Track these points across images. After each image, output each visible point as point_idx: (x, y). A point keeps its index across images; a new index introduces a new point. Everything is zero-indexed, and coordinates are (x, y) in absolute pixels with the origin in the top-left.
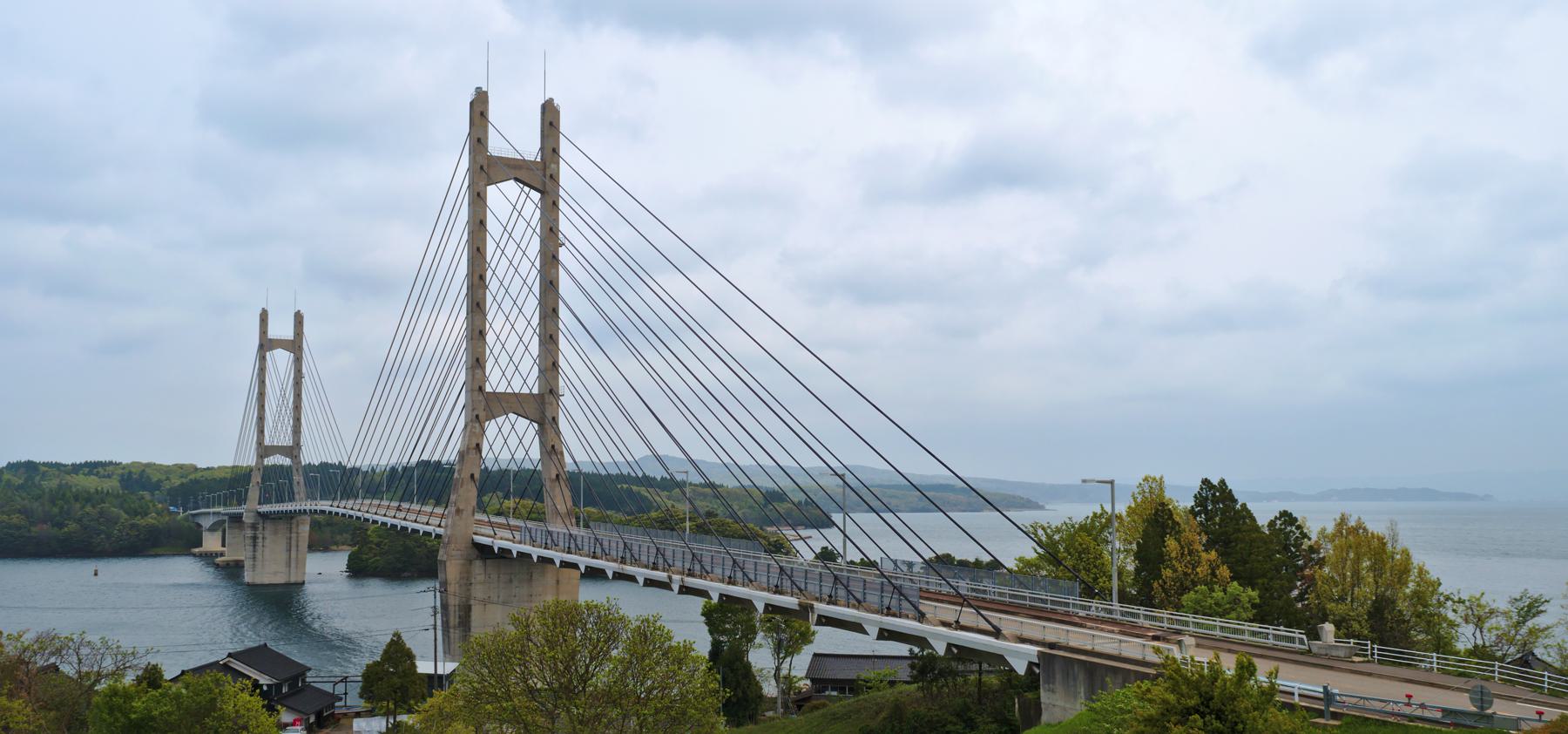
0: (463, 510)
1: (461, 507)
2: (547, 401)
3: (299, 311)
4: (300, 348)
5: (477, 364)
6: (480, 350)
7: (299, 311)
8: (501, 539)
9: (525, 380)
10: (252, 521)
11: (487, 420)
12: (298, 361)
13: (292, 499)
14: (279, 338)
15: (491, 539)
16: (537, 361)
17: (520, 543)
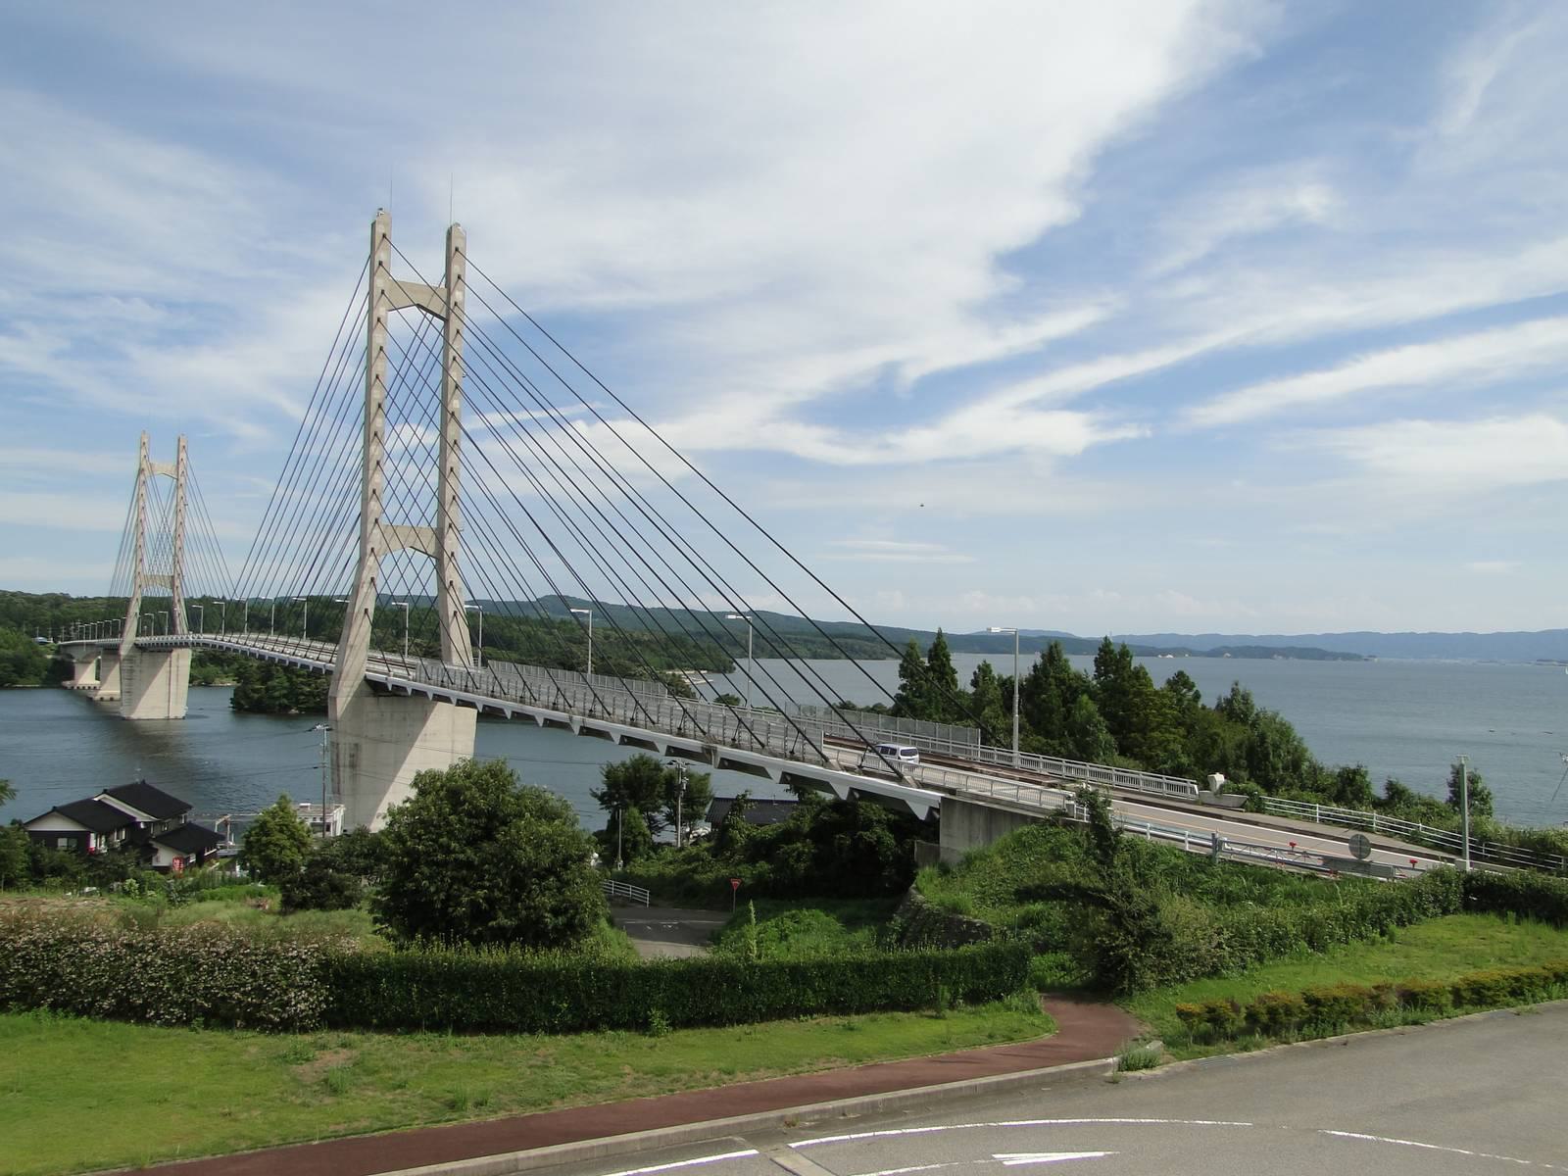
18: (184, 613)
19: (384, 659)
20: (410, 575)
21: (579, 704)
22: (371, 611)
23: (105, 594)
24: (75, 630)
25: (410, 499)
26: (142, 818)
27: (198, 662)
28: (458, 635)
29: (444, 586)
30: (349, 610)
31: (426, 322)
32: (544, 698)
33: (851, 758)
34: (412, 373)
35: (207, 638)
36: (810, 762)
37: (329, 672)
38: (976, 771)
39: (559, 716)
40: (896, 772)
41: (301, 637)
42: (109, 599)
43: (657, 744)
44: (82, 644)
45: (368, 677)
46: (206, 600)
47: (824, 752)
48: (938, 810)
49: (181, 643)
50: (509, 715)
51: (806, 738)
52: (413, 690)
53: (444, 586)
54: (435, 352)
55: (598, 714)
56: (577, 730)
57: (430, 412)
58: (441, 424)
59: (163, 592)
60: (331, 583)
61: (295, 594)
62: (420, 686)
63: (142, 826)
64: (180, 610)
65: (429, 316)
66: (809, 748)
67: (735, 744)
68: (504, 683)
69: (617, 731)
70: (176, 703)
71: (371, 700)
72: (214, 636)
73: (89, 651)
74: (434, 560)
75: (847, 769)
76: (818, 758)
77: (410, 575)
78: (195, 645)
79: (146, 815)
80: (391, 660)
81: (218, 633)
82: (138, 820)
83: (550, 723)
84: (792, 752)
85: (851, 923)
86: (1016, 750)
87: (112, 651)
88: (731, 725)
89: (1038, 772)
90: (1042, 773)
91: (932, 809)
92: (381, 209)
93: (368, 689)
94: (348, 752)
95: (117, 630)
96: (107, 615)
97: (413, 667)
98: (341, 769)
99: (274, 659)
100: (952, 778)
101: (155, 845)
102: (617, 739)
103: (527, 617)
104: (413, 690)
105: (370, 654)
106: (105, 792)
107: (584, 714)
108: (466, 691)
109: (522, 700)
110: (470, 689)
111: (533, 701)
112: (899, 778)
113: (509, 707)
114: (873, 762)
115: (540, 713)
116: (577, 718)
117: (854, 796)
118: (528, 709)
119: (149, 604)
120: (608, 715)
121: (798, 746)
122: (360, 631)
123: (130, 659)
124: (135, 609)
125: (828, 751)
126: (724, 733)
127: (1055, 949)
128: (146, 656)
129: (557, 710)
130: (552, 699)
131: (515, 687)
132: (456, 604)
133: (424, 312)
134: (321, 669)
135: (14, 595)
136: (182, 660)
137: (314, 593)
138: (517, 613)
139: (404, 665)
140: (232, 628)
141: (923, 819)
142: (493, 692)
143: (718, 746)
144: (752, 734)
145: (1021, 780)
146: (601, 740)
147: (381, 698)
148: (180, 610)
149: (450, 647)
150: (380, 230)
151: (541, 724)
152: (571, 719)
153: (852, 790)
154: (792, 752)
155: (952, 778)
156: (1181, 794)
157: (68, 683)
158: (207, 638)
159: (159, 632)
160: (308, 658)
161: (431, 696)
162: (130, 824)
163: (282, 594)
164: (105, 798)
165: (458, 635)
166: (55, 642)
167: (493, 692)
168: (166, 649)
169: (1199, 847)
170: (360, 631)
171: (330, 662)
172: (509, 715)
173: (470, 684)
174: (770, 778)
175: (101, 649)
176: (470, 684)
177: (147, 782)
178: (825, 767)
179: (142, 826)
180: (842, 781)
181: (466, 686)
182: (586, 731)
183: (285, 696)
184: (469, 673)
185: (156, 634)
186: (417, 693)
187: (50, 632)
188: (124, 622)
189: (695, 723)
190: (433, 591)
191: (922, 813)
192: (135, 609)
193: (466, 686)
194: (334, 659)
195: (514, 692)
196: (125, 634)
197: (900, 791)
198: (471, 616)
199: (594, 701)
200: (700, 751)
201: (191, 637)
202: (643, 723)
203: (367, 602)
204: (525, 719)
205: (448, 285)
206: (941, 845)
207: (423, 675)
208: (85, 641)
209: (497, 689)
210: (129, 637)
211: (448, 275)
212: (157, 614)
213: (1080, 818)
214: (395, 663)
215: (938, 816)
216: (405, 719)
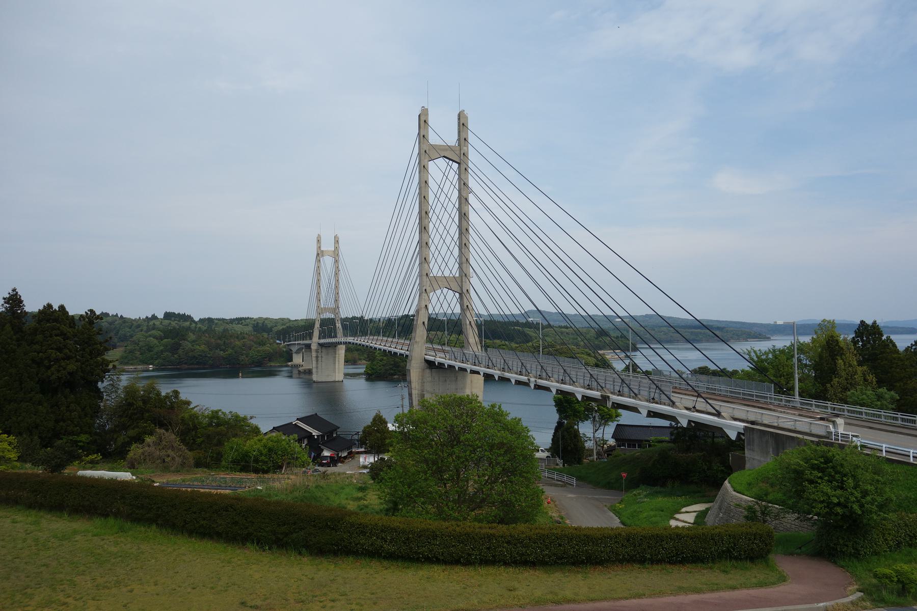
18: (340, 327)
20: (445, 306)
21: (534, 372)
22: (426, 323)
24: (293, 336)
25: (444, 264)
26: (315, 433)
28: (472, 337)
29: (465, 308)
30: (415, 323)
32: (515, 369)
33: (689, 401)
34: (443, 196)
36: (665, 404)
37: (407, 356)
38: (770, 410)
39: (523, 378)
40: (716, 411)
43: (576, 394)
44: (295, 344)
47: (672, 398)
48: (743, 434)
50: (497, 378)
51: (661, 391)
52: (459, 368)
53: (465, 308)
55: (545, 377)
56: (532, 386)
57: (452, 216)
59: (328, 315)
60: (407, 308)
62: (452, 363)
63: (316, 437)
64: (339, 325)
66: (663, 396)
67: (620, 394)
69: (554, 387)
70: (339, 373)
71: (428, 371)
73: (299, 347)
75: (687, 409)
76: (667, 401)
77: (445, 306)
78: (345, 343)
79: (316, 431)
82: (313, 434)
83: (518, 383)
84: (653, 399)
86: (797, 396)
87: (308, 347)
88: (645, 387)
89: (813, 410)
90: (815, 411)
91: (739, 434)
92: (423, 107)
96: (304, 329)
99: (397, 353)
100: (753, 414)
101: (322, 447)
103: (518, 321)
104: (459, 368)
105: (427, 346)
106: (298, 419)
109: (504, 370)
111: (527, 373)
112: (718, 414)
113: (496, 373)
114: (701, 404)
115: (513, 377)
116: (532, 379)
117: (691, 425)
118: (507, 375)
119: (324, 322)
120: (548, 378)
121: (657, 396)
122: (420, 333)
124: (317, 325)
125: (675, 397)
126: (614, 388)
128: (324, 350)
130: (519, 370)
131: (499, 362)
132: (470, 318)
133: (447, 160)
135: (266, 319)
136: (341, 351)
138: (512, 319)
140: (364, 333)
141: (734, 439)
144: (630, 388)
145: (800, 415)
147: (433, 370)
148: (339, 325)
149: (341, 437)
150: (423, 119)
151: (514, 383)
152: (529, 380)
153: (690, 421)
154: (653, 399)
155: (753, 414)
156: (912, 425)
159: (330, 337)
160: (397, 349)
161: (469, 371)
162: (310, 436)
165: (472, 337)
167: (488, 365)
168: (334, 345)
169: (903, 457)
170: (420, 333)
172: (497, 378)
173: (477, 362)
175: (304, 346)
176: (477, 362)
177: (318, 414)
178: (635, 399)
179: (316, 437)
180: (683, 416)
182: (538, 387)
183: (391, 369)
189: (597, 382)
190: (458, 310)
191: (733, 436)
192: (317, 325)
197: (673, 411)
198: (479, 326)
200: (600, 398)
201: (343, 340)
202: (568, 382)
203: (423, 318)
204: (503, 380)
205: (459, 145)
206: (746, 455)
207: (453, 357)
208: (296, 342)
210: (315, 340)
211: (459, 140)
212: (328, 327)
213: (837, 440)
214: (439, 350)
215: (743, 438)
216: (446, 381)
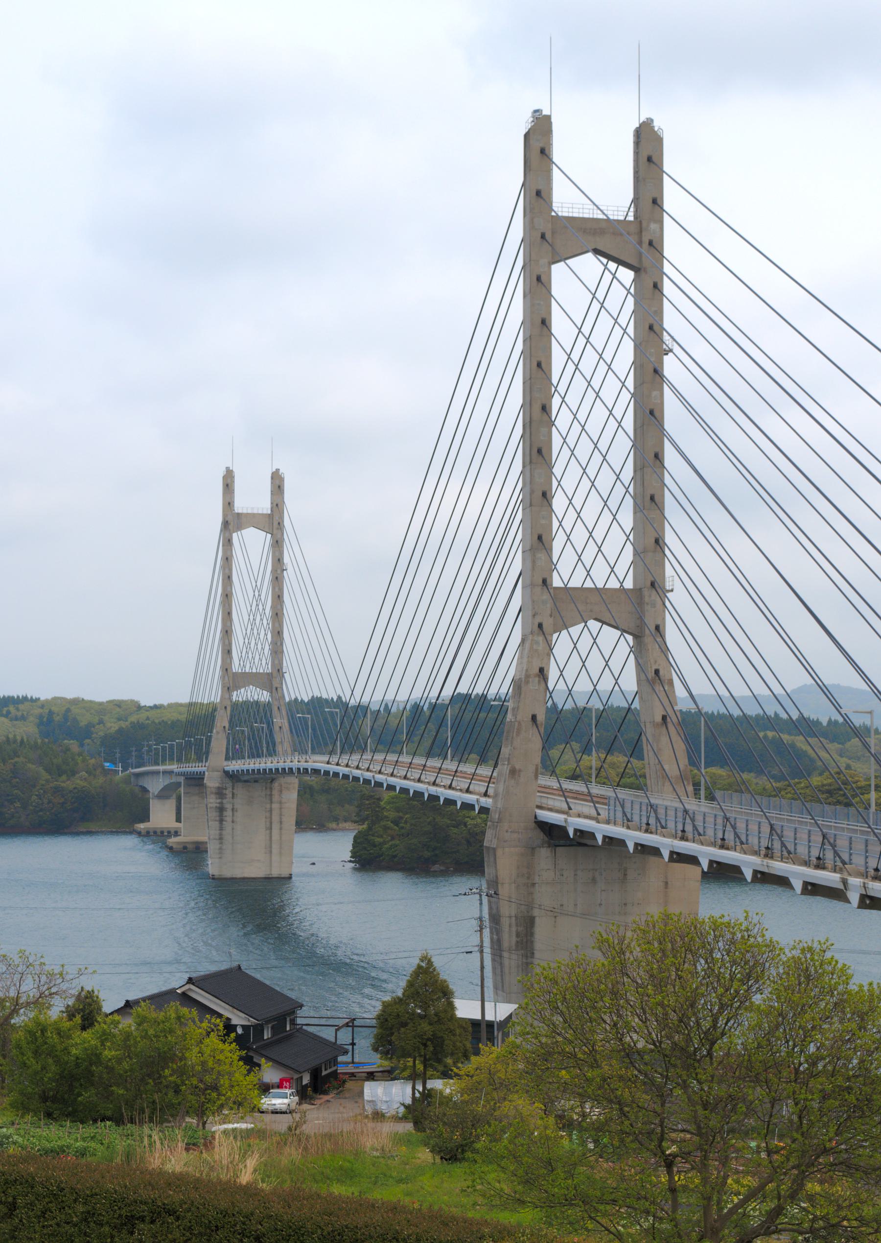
0: (520, 771)
1: (517, 767)
2: (647, 599)
3: (278, 470)
4: (280, 525)
5: (227, 652)
6: (543, 522)
7: (278, 470)
8: (579, 816)
9: (263, 665)
10: (217, 785)
11: (555, 632)
12: (277, 544)
13: (272, 752)
14: (250, 511)
15: (562, 817)
16: (631, 537)
17: (608, 822)
19: (561, 789)
20: (595, 664)
21: (858, 861)
23: (185, 699)
27: (305, 792)
31: (608, 277)
35: (319, 762)
39: (829, 878)
41: (445, 758)
42: (190, 705)
44: (157, 773)
45: (540, 819)
46: (317, 703)
49: (284, 769)
54: (623, 321)
56: (854, 897)
58: (635, 430)
61: (434, 693)
62: (617, 831)
64: (280, 721)
65: (612, 266)
68: (741, 826)
69: (797, 875)
71: (544, 853)
72: (325, 758)
74: (630, 638)
77: (595, 664)
80: (571, 791)
81: (331, 753)
83: (812, 889)
85: (415, 1130)
93: (541, 836)
94: (514, 929)
95: (203, 754)
97: (604, 800)
98: (505, 954)
102: (798, 885)
107: (865, 875)
108: (683, 838)
110: (690, 836)
116: (855, 881)
118: (779, 867)
123: (220, 793)
127: (594, 1207)
128: (240, 790)
129: (823, 868)
133: (605, 261)
134: (423, 794)
137: (463, 689)
139: (590, 797)
142: (723, 839)
143: (502, 783)
146: (779, 889)
152: (844, 882)
157: (141, 826)
158: (319, 762)
159: (256, 754)
163: (417, 695)
164: (190, 989)
166: (125, 769)
171: (486, 794)
173: (689, 828)
174: (850, 903)
181: (683, 831)
184: (686, 811)
185: (252, 756)
186: (610, 840)
187: (118, 755)
188: (209, 740)
192: (222, 721)
193: (683, 831)
194: (491, 792)
195: (756, 841)
196: (210, 756)
199: (823, 844)
201: (296, 762)
207: (619, 814)
209: (730, 836)
214: (577, 795)
216: (594, 880)
